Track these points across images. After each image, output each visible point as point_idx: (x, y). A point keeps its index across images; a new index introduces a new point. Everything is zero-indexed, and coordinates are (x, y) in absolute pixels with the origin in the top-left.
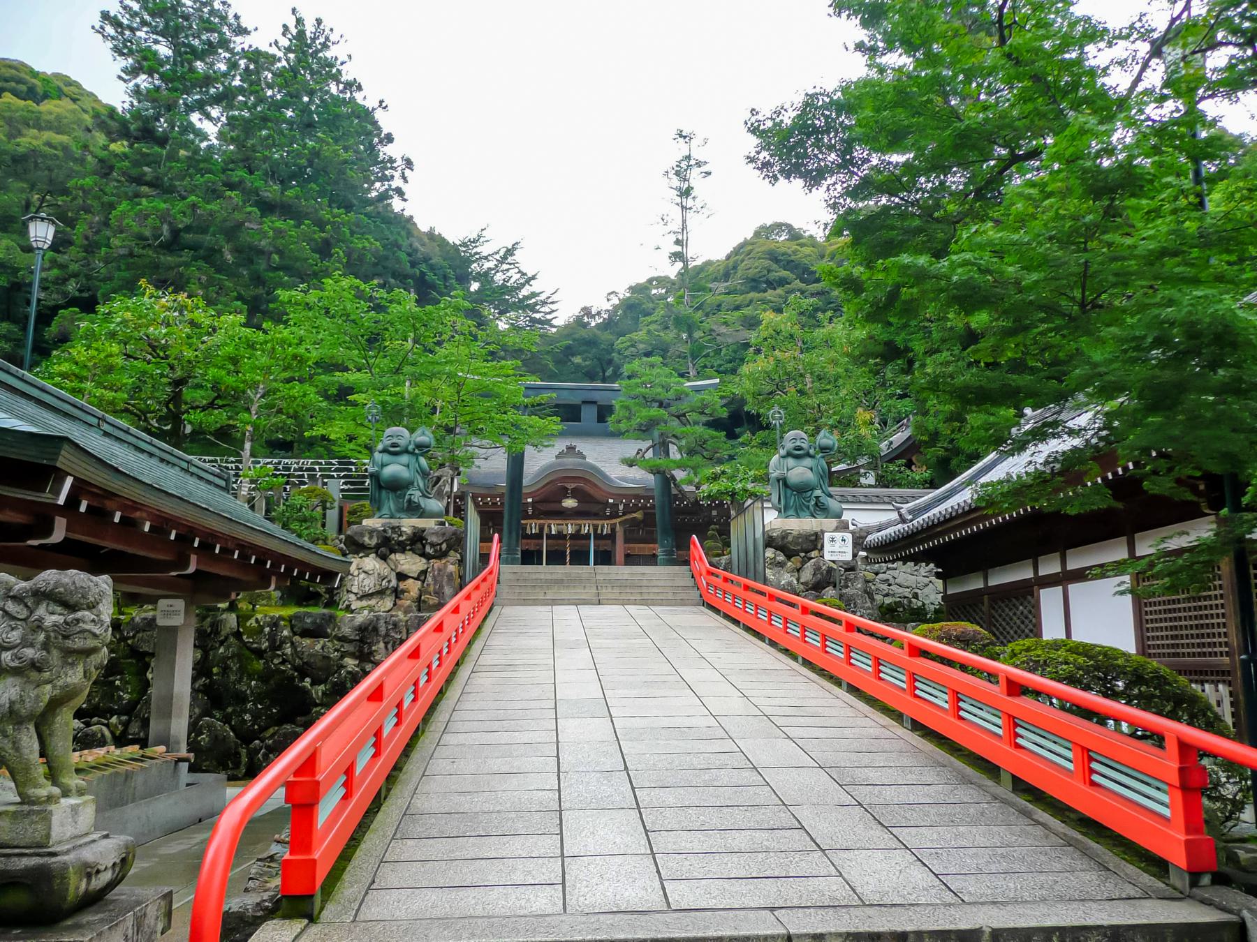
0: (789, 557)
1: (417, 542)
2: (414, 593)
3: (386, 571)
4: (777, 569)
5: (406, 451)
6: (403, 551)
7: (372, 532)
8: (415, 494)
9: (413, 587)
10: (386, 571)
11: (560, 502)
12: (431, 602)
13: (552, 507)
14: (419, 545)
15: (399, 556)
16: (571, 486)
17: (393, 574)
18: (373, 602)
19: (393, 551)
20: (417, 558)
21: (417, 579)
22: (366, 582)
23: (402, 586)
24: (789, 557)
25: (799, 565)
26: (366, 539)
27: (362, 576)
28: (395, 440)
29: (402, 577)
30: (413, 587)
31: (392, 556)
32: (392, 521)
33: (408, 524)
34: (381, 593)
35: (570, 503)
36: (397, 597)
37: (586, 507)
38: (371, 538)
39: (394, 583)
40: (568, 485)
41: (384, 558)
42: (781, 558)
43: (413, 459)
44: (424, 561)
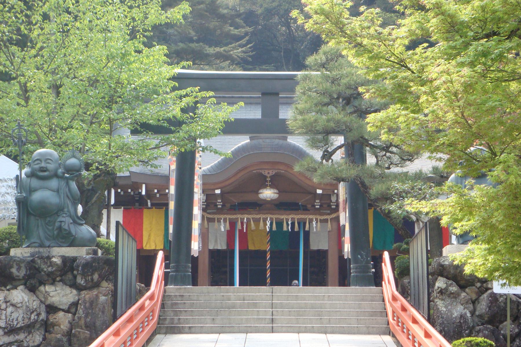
0: (463, 287)
1: (67, 272)
2: (64, 326)
3: (35, 304)
4: (448, 301)
5: (56, 175)
6: (53, 283)
7: (19, 262)
8: (66, 221)
9: (63, 320)
10: (35, 304)
11: (258, 193)
12: (82, 336)
13: (249, 198)
14: (70, 276)
15: (49, 288)
16: (269, 173)
17: (43, 307)
18: (21, 336)
19: (42, 283)
20: (68, 290)
21: (67, 311)
22: (15, 315)
23: (52, 318)
24: (463, 287)
25: (474, 297)
26: (14, 270)
27: (10, 309)
28: (43, 165)
29: (52, 309)
30: (63, 320)
31: (42, 288)
32: (41, 250)
33: (59, 253)
34: (29, 328)
35: (268, 194)
36: (46, 331)
37: (289, 198)
38: (19, 269)
39: (43, 316)
40: (265, 173)
41: (32, 290)
42: (454, 288)
43: (63, 183)
44: (75, 292)
